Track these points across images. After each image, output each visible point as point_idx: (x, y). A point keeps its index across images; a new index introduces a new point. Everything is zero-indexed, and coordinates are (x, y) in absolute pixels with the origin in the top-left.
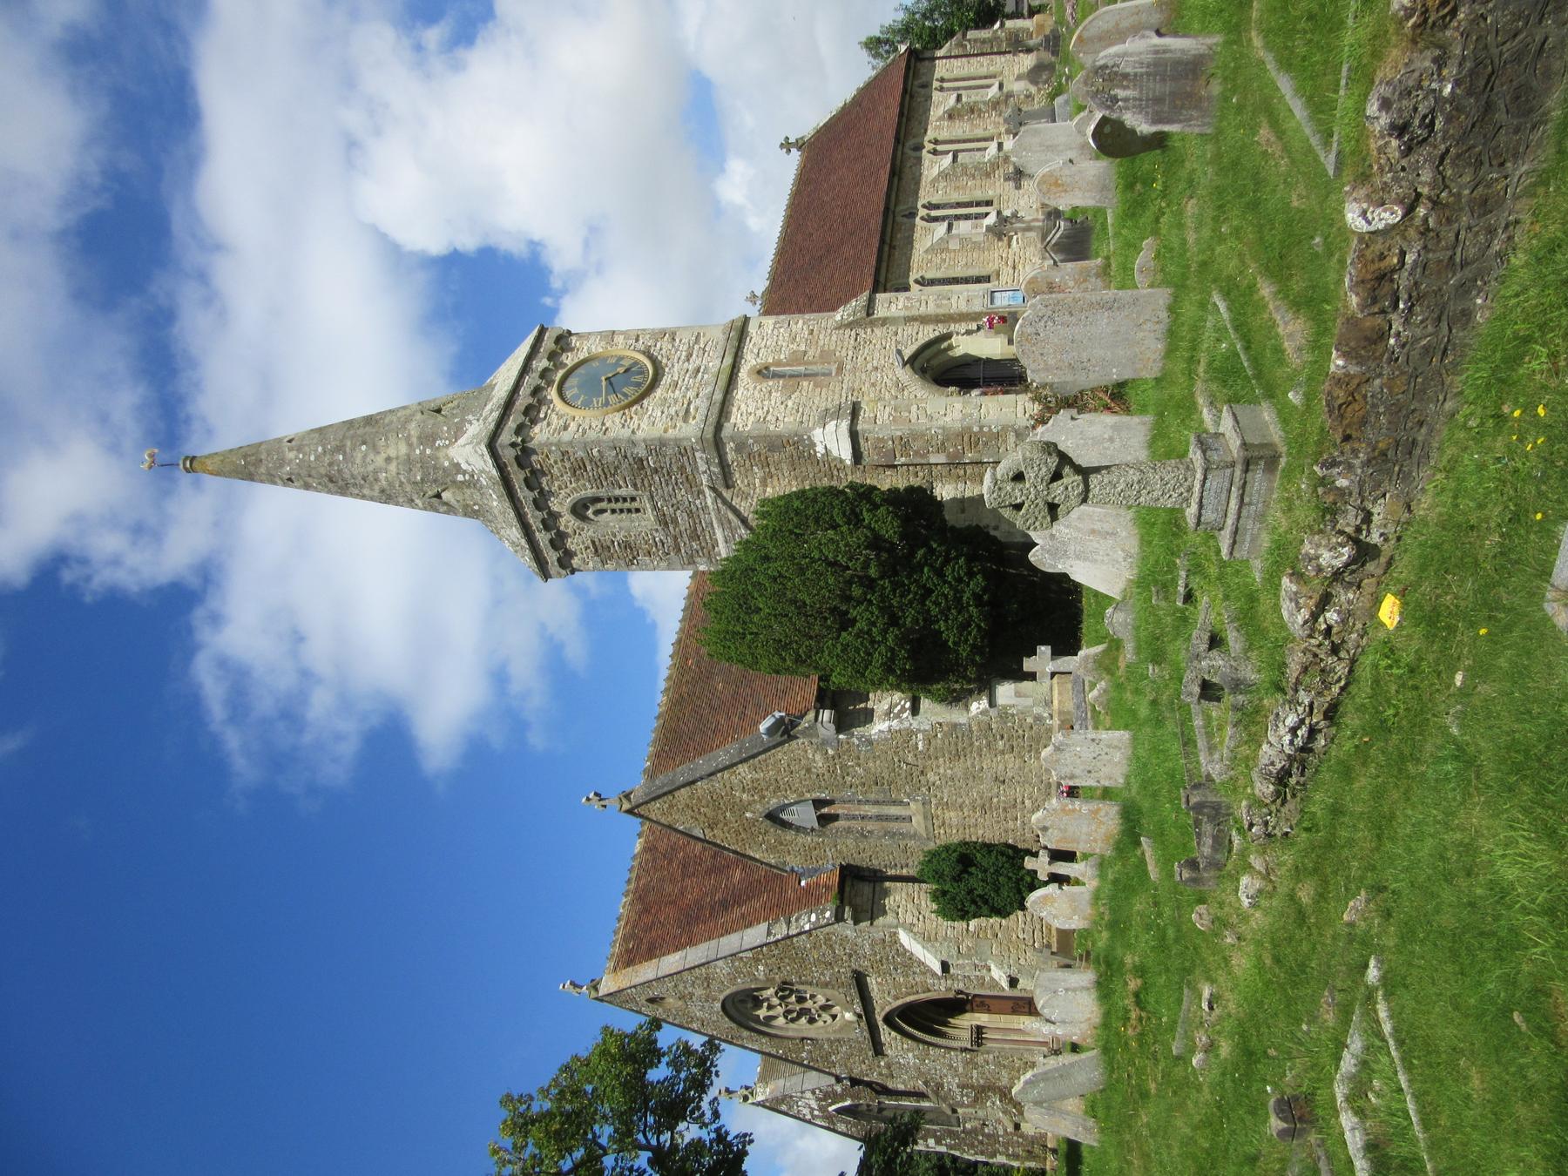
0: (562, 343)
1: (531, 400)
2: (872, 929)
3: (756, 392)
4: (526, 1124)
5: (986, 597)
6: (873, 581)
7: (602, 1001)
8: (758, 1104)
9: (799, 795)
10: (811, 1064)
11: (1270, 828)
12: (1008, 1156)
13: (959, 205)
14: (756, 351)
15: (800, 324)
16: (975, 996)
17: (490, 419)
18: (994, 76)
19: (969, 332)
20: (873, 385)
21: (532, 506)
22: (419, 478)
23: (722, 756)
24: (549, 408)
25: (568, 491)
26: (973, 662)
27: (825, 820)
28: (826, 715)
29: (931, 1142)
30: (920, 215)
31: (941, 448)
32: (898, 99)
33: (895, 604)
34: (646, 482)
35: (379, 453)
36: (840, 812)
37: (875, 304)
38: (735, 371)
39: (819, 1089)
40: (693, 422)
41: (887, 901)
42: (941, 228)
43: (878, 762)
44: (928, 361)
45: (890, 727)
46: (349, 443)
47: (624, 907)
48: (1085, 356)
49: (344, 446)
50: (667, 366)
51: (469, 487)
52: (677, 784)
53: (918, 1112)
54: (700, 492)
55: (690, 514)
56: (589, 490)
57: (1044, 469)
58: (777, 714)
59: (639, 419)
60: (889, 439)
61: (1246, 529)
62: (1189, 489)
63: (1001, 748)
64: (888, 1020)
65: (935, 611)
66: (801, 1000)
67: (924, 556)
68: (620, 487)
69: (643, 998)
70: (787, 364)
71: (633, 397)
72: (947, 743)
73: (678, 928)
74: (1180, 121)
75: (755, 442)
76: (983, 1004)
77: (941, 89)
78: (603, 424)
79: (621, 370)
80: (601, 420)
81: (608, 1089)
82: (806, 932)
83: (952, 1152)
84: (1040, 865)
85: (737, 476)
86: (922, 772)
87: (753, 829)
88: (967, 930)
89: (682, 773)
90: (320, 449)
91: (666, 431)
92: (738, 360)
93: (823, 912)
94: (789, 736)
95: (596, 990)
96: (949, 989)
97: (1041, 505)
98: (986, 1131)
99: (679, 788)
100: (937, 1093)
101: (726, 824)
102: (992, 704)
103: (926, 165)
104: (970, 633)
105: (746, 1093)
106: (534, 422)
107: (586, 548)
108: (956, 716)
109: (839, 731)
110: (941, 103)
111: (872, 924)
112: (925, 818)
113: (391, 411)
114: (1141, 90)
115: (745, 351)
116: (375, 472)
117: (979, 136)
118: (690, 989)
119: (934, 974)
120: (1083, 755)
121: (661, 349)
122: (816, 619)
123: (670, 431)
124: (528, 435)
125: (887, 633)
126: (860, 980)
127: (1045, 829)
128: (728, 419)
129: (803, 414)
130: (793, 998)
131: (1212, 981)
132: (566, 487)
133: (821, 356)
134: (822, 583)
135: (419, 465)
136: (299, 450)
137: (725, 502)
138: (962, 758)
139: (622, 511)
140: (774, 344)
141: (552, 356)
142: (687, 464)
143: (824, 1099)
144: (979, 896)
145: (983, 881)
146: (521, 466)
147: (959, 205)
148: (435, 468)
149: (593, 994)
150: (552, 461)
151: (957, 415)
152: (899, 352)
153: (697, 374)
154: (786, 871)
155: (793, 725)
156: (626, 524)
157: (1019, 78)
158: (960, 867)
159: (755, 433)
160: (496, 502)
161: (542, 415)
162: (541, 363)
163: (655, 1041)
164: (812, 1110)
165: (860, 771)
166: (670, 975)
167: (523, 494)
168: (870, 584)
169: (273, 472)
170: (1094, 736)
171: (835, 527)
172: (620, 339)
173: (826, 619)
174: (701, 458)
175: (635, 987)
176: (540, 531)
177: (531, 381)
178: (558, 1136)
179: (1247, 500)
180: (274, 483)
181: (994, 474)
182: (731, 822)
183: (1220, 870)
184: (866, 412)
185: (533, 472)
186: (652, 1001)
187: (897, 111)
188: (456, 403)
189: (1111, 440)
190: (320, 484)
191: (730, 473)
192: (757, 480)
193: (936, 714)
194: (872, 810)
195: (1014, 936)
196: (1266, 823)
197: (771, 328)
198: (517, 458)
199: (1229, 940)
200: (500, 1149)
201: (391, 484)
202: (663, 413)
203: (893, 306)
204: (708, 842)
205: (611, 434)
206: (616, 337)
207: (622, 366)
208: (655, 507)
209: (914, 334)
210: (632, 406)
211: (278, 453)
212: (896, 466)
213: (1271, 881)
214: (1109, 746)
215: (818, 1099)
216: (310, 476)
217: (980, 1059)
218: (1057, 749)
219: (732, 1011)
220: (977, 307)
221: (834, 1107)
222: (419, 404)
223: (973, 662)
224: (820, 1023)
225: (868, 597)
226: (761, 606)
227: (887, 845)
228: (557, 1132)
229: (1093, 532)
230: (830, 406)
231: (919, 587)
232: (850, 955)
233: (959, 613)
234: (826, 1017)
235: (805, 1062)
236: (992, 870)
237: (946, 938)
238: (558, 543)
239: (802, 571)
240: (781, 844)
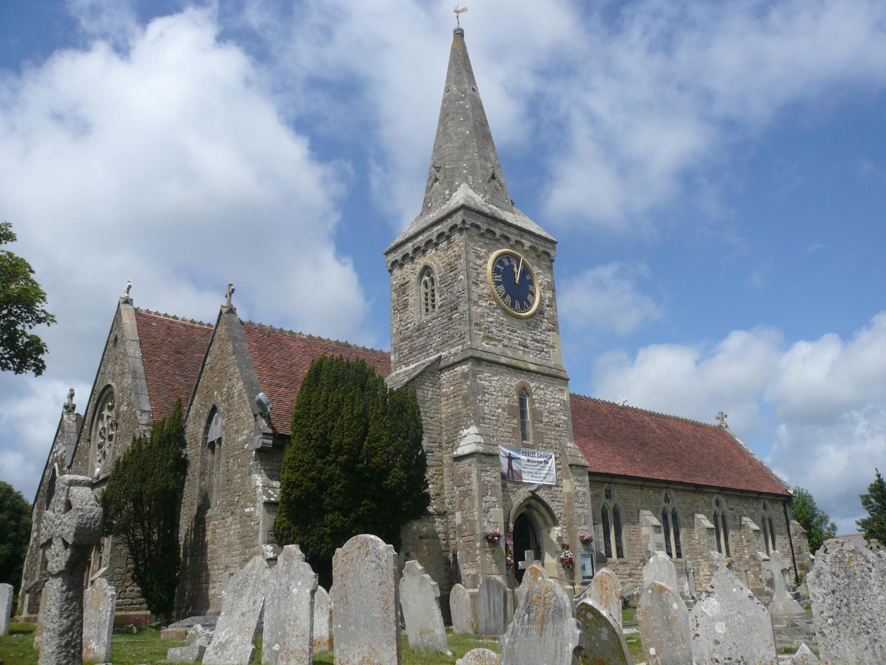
10: (78, 449)
34: (444, 313)
38: (525, 372)
45: (258, 486)
54: (438, 351)
55: (424, 346)
56: (438, 275)
59: (485, 307)
60: (470, 481)
68: (440, 296)
71: (503, 303)
107: (404, 278)
118: (119, 363)
129: (490, 419)
132: (440, 260)
133: (539, 433)
135: (456, 166)
140: (547, 399)
142: (454, 340)
153: (522, 346)
165: (236, 468)
174: (458, 349)
176: (413, 246)
185: (448, 237)
187: (744, 488)
188: (500, 188)
202: (491, 322)
208: (429, 322)
209: (557, 499)
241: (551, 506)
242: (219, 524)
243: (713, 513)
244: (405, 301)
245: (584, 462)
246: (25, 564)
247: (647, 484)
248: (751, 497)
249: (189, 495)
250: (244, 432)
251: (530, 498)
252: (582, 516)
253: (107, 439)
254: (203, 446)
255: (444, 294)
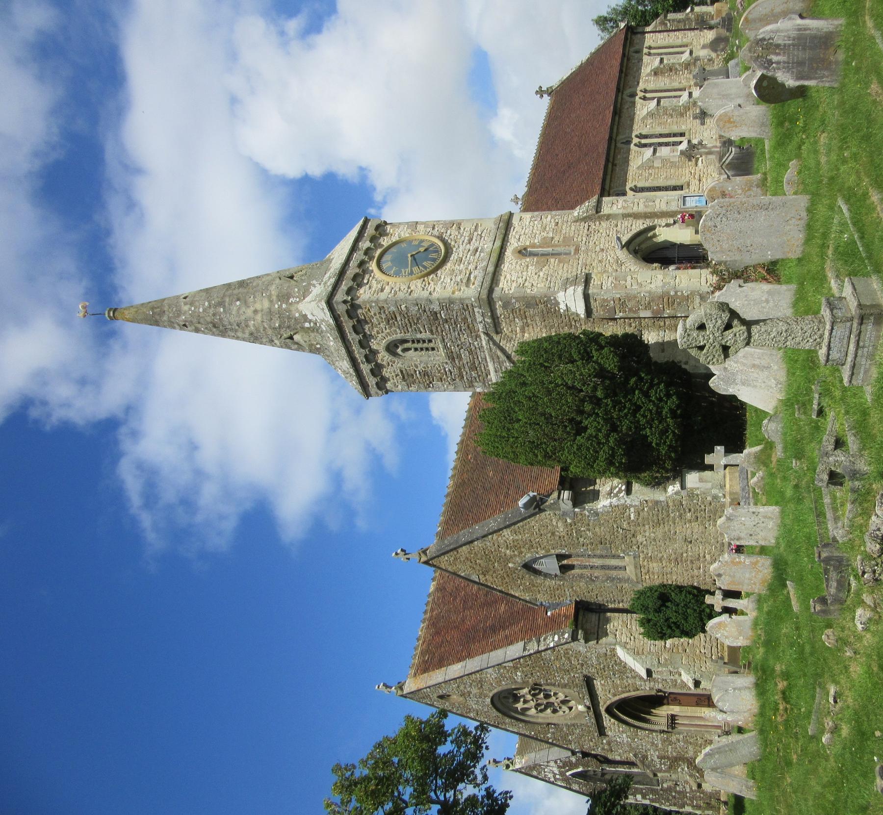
0: (380, 229)
1: (357, 270)
2: (598, 646)
3: (518, 266)
4: (350, 785)
5: (679, 412)
6: (599, 400)
7: (406, 697)
8: (517, 771)
9: (547, 551)
10: (554, 742)
11: (877, 575)
12: (693, 807)
13: (661, 136)
14: (517, 237)
15: (549, 218)
16: (670, 693)
17: (329, 283)
18: (686, 46)
19: (668, 225)
20: (600, 261)
21: (358, 345)
22: (277, 325)
23: (492, 524)
24: (370, 276)
25: (384, 335)
26: (670, 458)
27: (564, 569)
28: (566, 494)
29: (639, 797)
30: (634, 143)
31: (648, 306)
32: (619, 60)
33: (615, 416)
34: (439, 329)
35: (249, 307)
36: (575, 563)
37: (601, 205)
38: (503, 251)
39: (560, 759)
40: (473, 287)
41: (608, 626)
42: (649, 152)
43: (602, 528)
44: (639, 245)
46: (227, 300)
47: (422, 631)
48: (749, 243)
49: (224, 302)
50: (454, 246)
51: (313, 331)
52: (460, 543)
53: (629, 777)
54: (478, 336)
56: (399, 335)
57: (720, 322)
58: (531, 494)
59: (434, 284)
60: (611, 300)
61: (861, 365)
62: (821, 336)
63: (689, 518)
64: (609, 710)
65: (643, 421)
66: (547, 696)
67: (636, 382)
69: (435, 695)
70: (540, 247)
71: (431, 268)
72: (651, 515)
73: (461, 645)
74: (816, 78)
75: (517, 301)
76: (675, 699)
77: (649, 54)
78: (409, 288)
79: (422, 249)
80: (407, 285)
81: (410, 761)
82: (550, 648)
83: (654, 804)
84: (716, 601)
85: (504, 325)
86: (634, 535)
87: (514, 575)
88: (665, 647)
89: (464, 535)
90: (207, 304)
91: (453, 293)
92: (505, 243)
93: (563, 634)
94: (540, 509)
95: (401, 688)
96: (651, 689)
97: (717, 347)
98: (678, 789)
99: (461, 546)
100: (643, 762)
101: (494, 572)
102: (683, 487)
103: (638, 107)
104: (667, 437)
105: (508, 762)
106: (360, 286)
107: (397, 376)
108: (657, 495)
109: (575, 505)
110: (649, 64)
111: (597, 642)
112: (636, 567)
113: (258, 277)
114: (789, 57)
115: (510, 237)
116: (246, 320)
117: (676, 88)
118: (469, 689)
119: (641, 678)
120: (746, 523)
121: (450, 235)
122: (559, 426)
123: (457, 293)
124: (355, 295)
125: (609, 437)
126: (589, 682)
127: (719, 575)
128: (497, 285)
129: (550, 282)
130: (542, 695)
131: (837, 683)
132: (382, 332)
133: (564, 241)
134: (563, 401)
135: (277, 316)
136: (192, 304)
137: (495, 343)
138: (662, 525)
139: (422, 349)
140: (530, 232)
141: (373, 239)
142: (468, 316)
143: (564, 767)
144: (673, 623)
145: (676, 612)
146: (350, 317)
147: (661, 136)
148: (289, 318)
149: (400, 693)
150: (372, 314)
151: (659, 284)
152: (619, 239)
154: (537, 605)
155: (543, 501)
156: (425, 359)
157: (704, 47)
158: (660, 603)
159: (516, 295)
160: (332, 342)
161: (365, 281)
162: (365, 244)
163: (443, 726)
164: (555, 775)
165: (589, 534)
166: (455, 679)
167: (352, 336)
168: (597, 402)
169: (173, 320)
170: (754, 510)
171: (572, 361)
172: (421, 228)
173: (566, 427)
174: (478, 312)
175: (429, 687)
177: (358, 256)
178: (374, 794)
179: (861, 344)
180: (174, 328)
181: (684, 325)
182: (498, 570)
183: (842, 604)
184: (595, 281)
185: (359, 321)
186: (441, 697)
187: (618, 69)
188: (304, 272)
189: (767, 301)
190: (206, 328)
191: (499, 323)
192: (518, 328)
193: (643, 494)
194: (598, 562)
195: (698, 651)
196: (874, 572)
197: (528, 220)
198: (347, 311)
199: (848, 654)
200: (332, 803)
201: (257, 330)
202: (451, 280)
203: (615, 207)
204: (482, 585)
205: (415, 295)
206: (418, 226)
207: (423, 246)
208: (445, 347)
209: (629, 226)
210: (430, 275)
211: (176, 306)
212: (616, 319)
213: (877, 612)
214: (765, 517)
215: (559, 767)
216: (199, 323)
217: (674, 738)
218: (729, 519)
219: (499, 705)
220: (674, 207)
221: (570, 773)
222: (278, 272)
223: (670, 458)
224: (561, 713)
225: (596, 411)
226: (520, 418)
227: (608, 587)
228: (373, 792)
229: (754, 366)
230: (569, 276)
231: (631, 404)
232: (582, 665)
233: (660, 422)
234: (565, 708)
235: (550, 741)
236: (682, 605)
237: (650, 652)
238: (376, 372)
239: (549, 392)
240: (534, 586)
241: (636, 231)
242: (643, 552)
243: (642, 101)
244: (420, 375)
245: (594, 199)
246: (668, 808)
247: (611, 159)
248: (627, 65)
249: (611, 595)
250: (555, 524)
251: (628, 249)
252: (647, 204)
253: (548, 701)
254: (564, 579)
255: (418, 328)
